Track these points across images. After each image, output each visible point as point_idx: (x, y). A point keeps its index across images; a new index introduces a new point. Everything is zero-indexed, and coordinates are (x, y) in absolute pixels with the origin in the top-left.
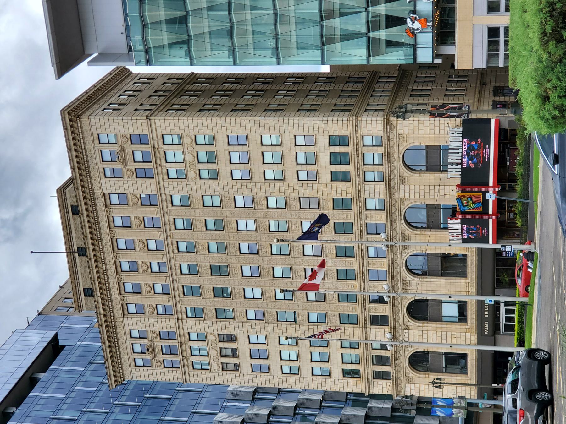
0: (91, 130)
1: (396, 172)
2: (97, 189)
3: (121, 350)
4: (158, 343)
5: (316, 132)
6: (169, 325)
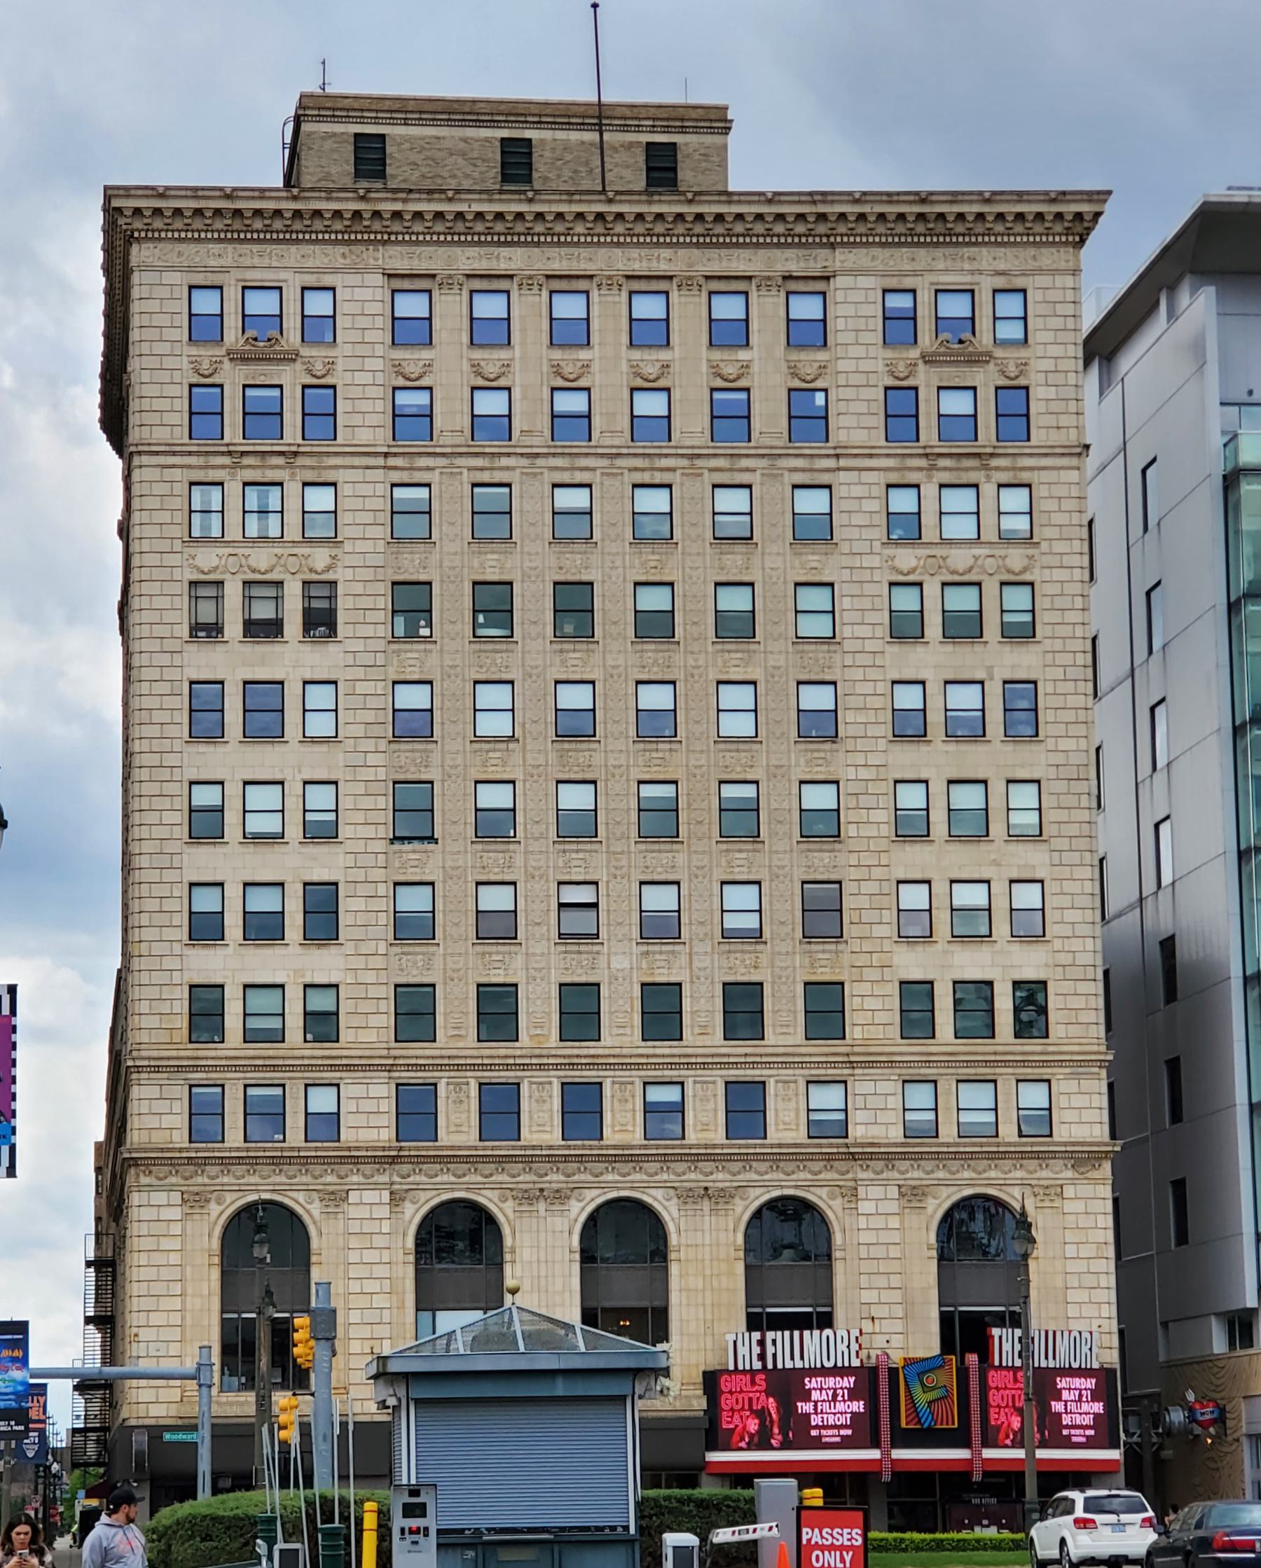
0: (1040, 271)
1: (941, 1174)
2: (841, 258)
3: (256, 248)
4: (291, 378)
5: (1057, 944)
6: (363, 420)
